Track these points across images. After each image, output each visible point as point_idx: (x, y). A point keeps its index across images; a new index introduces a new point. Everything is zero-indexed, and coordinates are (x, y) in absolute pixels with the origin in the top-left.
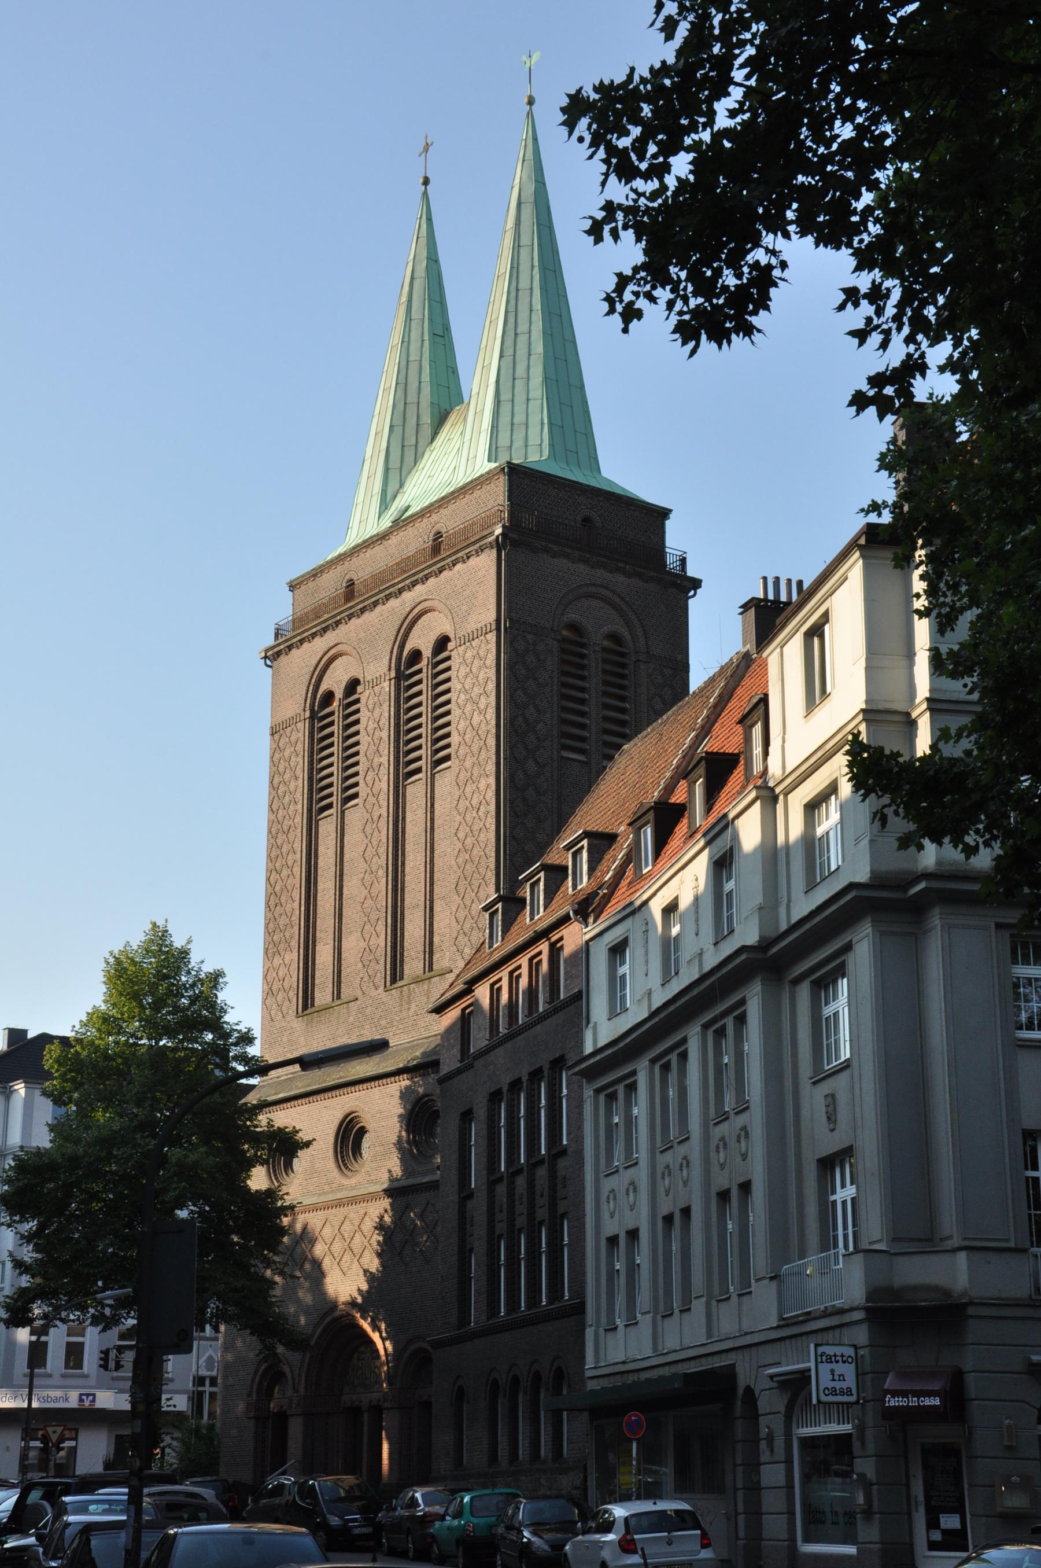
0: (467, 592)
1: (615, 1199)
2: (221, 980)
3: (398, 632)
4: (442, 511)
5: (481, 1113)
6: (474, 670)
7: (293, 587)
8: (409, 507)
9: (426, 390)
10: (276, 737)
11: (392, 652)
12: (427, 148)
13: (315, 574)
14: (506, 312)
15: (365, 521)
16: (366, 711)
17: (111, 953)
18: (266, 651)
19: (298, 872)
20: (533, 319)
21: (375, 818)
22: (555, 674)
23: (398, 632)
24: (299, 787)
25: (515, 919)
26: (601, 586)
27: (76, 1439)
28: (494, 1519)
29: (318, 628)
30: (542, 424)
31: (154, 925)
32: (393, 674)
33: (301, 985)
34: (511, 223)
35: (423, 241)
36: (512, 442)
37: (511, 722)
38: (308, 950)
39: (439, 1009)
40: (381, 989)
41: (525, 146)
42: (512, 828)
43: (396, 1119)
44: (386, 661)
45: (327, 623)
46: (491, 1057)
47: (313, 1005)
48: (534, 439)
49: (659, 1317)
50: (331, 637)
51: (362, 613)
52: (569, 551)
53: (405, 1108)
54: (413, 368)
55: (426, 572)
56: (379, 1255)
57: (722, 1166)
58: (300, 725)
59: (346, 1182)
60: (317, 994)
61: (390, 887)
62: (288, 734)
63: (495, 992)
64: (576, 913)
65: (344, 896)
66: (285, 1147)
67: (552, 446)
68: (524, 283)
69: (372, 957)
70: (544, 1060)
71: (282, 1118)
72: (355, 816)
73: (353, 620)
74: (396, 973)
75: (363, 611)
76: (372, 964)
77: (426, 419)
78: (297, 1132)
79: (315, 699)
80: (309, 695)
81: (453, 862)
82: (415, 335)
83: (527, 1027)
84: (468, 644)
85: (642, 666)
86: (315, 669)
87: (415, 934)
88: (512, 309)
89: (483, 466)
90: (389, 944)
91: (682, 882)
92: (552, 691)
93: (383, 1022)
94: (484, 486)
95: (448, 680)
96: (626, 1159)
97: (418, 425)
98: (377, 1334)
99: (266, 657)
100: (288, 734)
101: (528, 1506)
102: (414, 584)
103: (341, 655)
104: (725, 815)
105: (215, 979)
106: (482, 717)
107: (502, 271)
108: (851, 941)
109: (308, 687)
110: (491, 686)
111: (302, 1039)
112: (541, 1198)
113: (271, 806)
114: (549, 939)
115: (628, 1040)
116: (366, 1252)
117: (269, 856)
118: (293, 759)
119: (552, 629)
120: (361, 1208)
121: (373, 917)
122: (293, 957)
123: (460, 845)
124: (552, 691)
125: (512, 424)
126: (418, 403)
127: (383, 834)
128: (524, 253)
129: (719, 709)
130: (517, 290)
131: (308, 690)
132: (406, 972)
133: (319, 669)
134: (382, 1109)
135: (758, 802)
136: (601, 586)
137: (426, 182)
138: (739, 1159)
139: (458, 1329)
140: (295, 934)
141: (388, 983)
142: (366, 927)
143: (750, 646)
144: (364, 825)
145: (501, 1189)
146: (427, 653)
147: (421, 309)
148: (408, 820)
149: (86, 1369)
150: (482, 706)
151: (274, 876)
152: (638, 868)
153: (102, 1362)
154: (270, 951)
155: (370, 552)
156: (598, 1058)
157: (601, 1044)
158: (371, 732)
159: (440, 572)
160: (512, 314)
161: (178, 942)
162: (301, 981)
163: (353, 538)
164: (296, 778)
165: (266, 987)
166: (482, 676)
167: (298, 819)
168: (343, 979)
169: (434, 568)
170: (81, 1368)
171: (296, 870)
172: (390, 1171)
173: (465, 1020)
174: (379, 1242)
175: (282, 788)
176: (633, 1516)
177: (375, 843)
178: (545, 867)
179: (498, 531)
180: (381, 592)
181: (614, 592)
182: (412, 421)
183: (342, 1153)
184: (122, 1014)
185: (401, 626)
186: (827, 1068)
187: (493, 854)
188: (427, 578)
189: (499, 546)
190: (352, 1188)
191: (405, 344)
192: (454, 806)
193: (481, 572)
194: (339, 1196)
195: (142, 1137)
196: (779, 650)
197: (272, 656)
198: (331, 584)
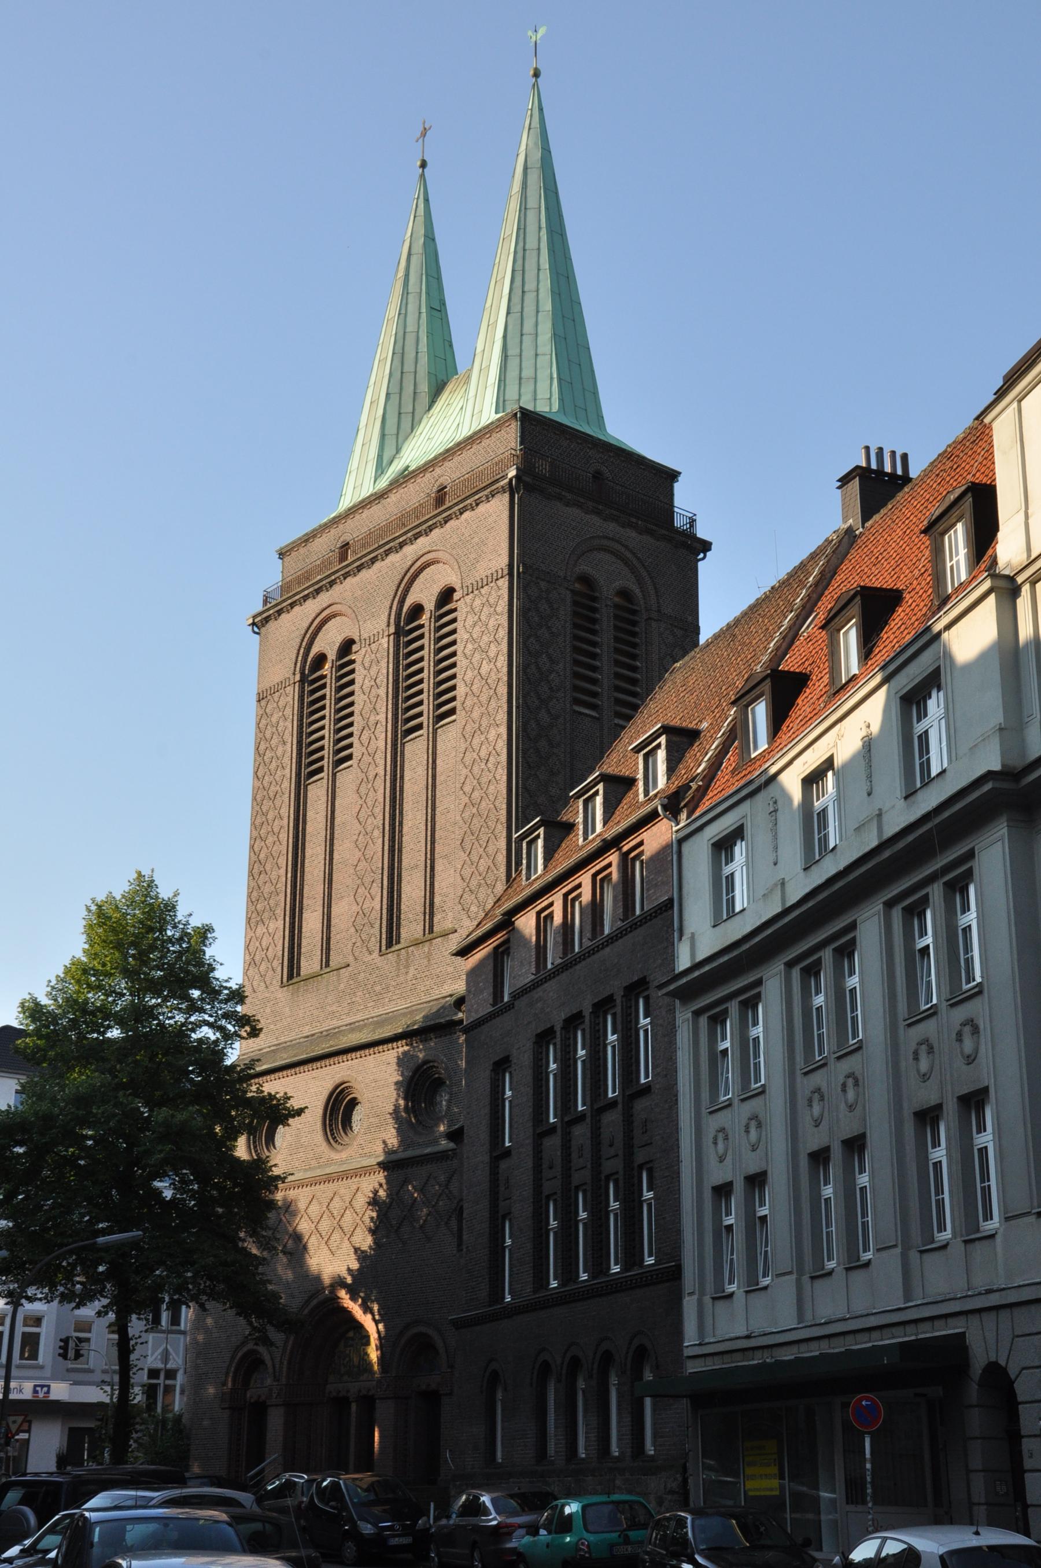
0: (476, 540)
1: (726, 1138)
2: (209, 935)
3: (399, 587)
4: (446, 464)
5: (523, 1057)
6: (483, 618)
7: (282, 555)
8: (408, 467)
9: (424, 359)
10: (263, 703)
11: (391, 608)
12: (424, 133)
13: (307, 539)
14: (513, 271)
15: (359, 482)
16: (362, 670)
17: (93, 900)
18: (254, 617)
19: (286, 838)
20: (541, 277)
21: (371, 777)
22: (568, 624)
23: (399, 587)
24: (287, 751)
25: (559, 846)
26: (612, 539)
27: (28, 1431)
28: (616, 1535)
29: (311, 589)
30: (552, 378)
31: (139, 874)
32: (392, 630)
33: (286, 954)
34: (517, 187)
35: (421, 219)
36: (520, 395)
37: (524, 669)
38: (294, 918)
39: (464, 952)
40: (376, 954)
41: (531, 116)
42: (525, 780)
43: (393, 1087)
44: (384, 618)
45: (321, 584)
46: (538, 993)
47: (298, 974)
48: (543, 392)
49: (806, 1278)
50: (324, 599)
51: (359, 571)
52: (582, 500)
53: (402, 1075)
54: (410, 340)
55: (431, 523)
56: (373, 1232)
57: (925, 1077)
58: (289, 689)
59: (334, 1156)
60: (303, 963)
61: (386, 847)
62: (276, 699)
63: (544, 921)
64: (665, 808)
65: (334, 861)
66: (276, 1113)
67: (561, 400)
68: (531, 243)
69: (366, 921)
70: (616, 987)
71: (272, 1086)
72: (348, 778)
73: (348, 579)
74: (392, 936)
75: (359, 569)
76: (366, 928)
77: (424, 387)
78: (289, 1098)
79: (306, 662)
80: (300, 658)
81: (458, 818)
82: (412, 308)
83: (587, 954)
84: (476, 592)
85: (654, 624)
86: (307, 632)
87: (414, 895)
88: (519, 267)
89: (489, 415)
90: (385, 907)
91: (840, 736)
92: (565, 641)
93: (378, 988)
94: (494, 435)
95: (454, 632)
96: (743, 1090)
97: (415, 393)
98: (369, 1316)
99: (253, 624)
100: (276, 699)
101: (697, 1522)
102: (417, 536)
103: (334, 616)
104: (928, 629)
105: (204, 933)
106: (492, 665)
107: (508, 233)
108: (855, 921)
109: (299, 650)
110: (503, 633)
111: (287, 1009)
112: (623, 1144)
113: (256, 773)
114: (620, 849)
115: (757, 939)
116: (358, 1230)
117: (253, 824)
118: (281, 724)
119: (565, 578)
120: (353, 1183)
121: (367, 880)
122: (278, 926)
123: (466, 800)
124: (565, 641)
125: (520, 378)
126: (415, 372)
127: (380, 791)
128: (531, 216)
129: (820, 588)
130: (524, 250)
131: (298, 654)
132: (403, 935)
133: (310, 632)
134: (377, 1080)
135: (992, 597)
136: (612, 539)
137: (424, 165)
138: (959, 1063)
139: (490, 1306)
140: (281, 902)
141: (384, 948)
142: (359, 890)
143: (854, 521)
144: (356, 792)
145: (553, 1144)
146: (429, 605)
147: (419, 283)
148: (406, 778)
149: (41, 1360)
150: (492, 654)
151: (258, 844)
152: (745, 749)
153: (61, 1351)
154: (253, 920)
155: (366, 513)
156: (697, 974)
157: (701, 956)
158: (367, 691)
159: (446, 522)
160: (519, 273)
161: (165, 893)
162: (286, 950)
163: (346, 502)
164: (284, 743)
165: (247, 958)
166: (492, 623)
167: (286, 784)
168: (332, 946)
169: (439, 518)
170: (36, 1359)
171: (283, 836)
172: (384, 1142)
173: (500, 955)
174: (372, 1218)
175: (269, 754)
176: (952, 1553)
177: (370, 804)
178: (604, 778)
179: (512, 473)
180: (380, 547)
181: (626, 547)
182: (409, 389)
183: (331, 1125)
184: (104, 965)
185: (402, 581)
186: (965, 987)
187: (504, 806)
188: (431, 529)
189: (511, 489)
190: (342, 1162)
191: (402, 316)
192: (459, 759)
193: (495, 515)
194: (328, 1171)
195: (125, 1095)
196: (1015, 404)
197: (260, 623)
198: (324, 546)
